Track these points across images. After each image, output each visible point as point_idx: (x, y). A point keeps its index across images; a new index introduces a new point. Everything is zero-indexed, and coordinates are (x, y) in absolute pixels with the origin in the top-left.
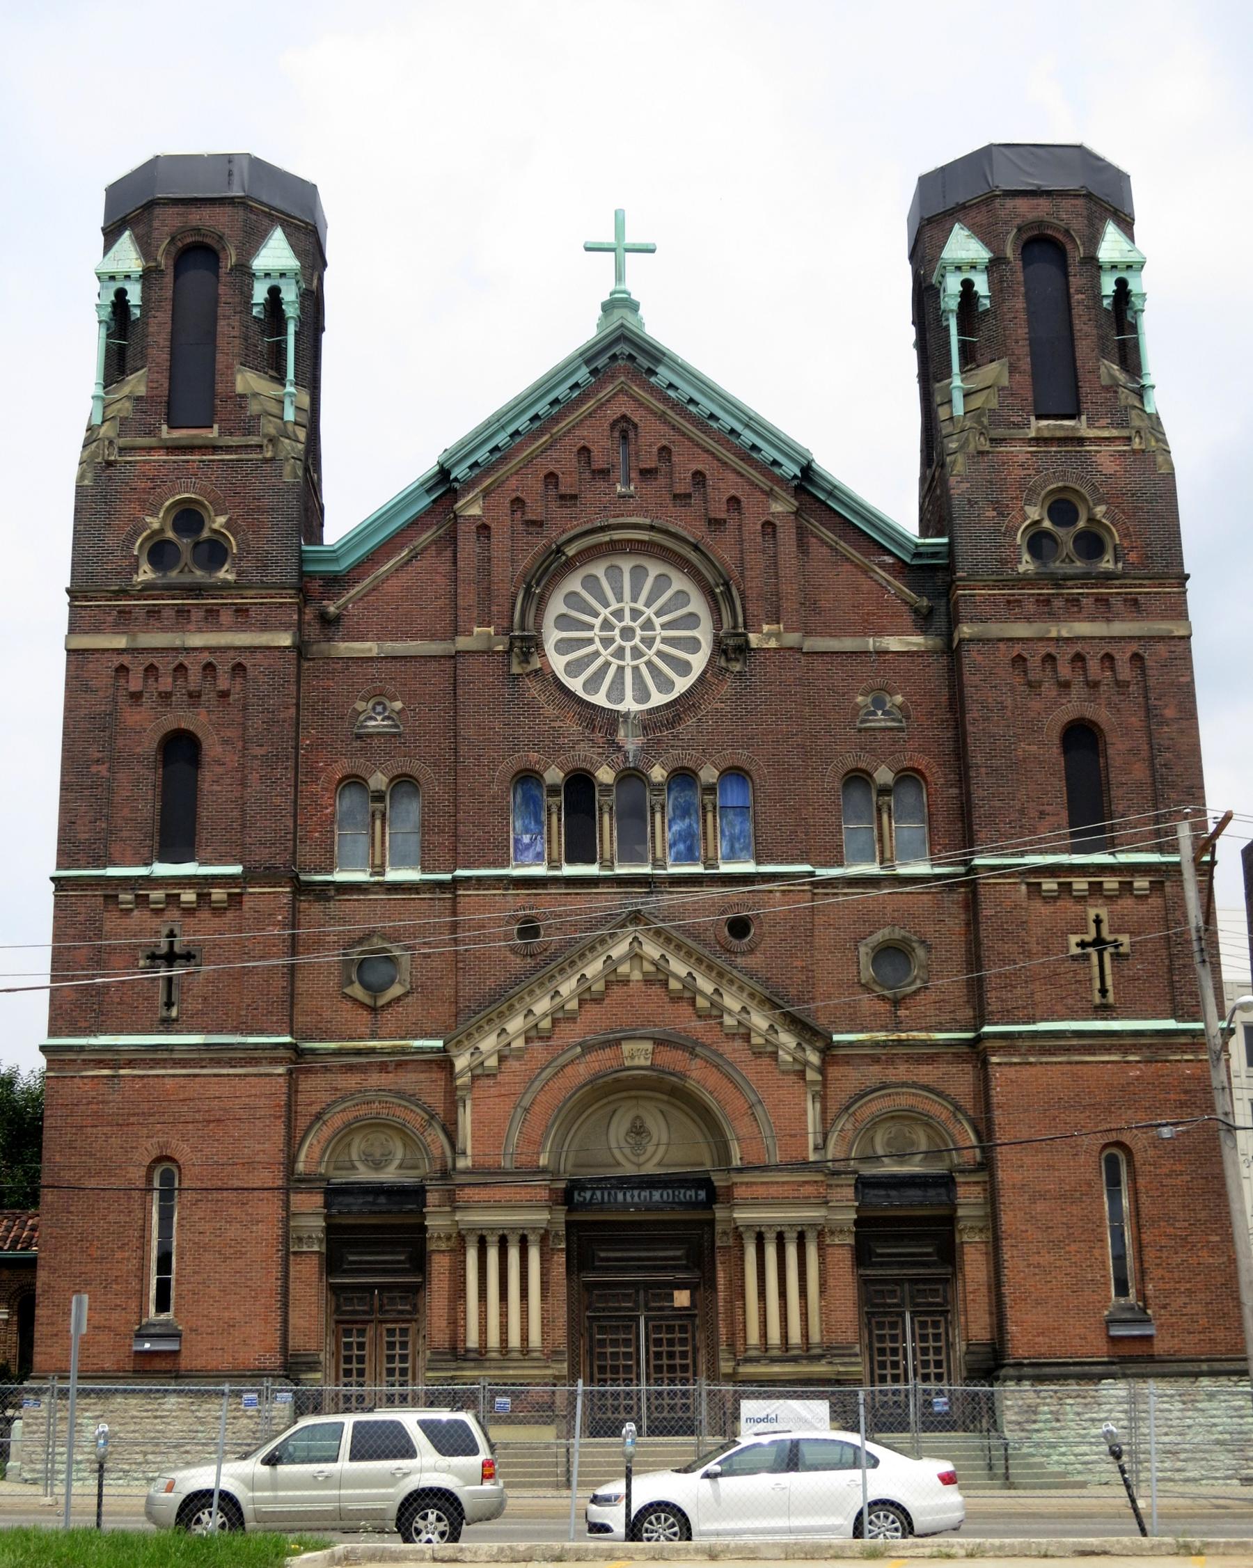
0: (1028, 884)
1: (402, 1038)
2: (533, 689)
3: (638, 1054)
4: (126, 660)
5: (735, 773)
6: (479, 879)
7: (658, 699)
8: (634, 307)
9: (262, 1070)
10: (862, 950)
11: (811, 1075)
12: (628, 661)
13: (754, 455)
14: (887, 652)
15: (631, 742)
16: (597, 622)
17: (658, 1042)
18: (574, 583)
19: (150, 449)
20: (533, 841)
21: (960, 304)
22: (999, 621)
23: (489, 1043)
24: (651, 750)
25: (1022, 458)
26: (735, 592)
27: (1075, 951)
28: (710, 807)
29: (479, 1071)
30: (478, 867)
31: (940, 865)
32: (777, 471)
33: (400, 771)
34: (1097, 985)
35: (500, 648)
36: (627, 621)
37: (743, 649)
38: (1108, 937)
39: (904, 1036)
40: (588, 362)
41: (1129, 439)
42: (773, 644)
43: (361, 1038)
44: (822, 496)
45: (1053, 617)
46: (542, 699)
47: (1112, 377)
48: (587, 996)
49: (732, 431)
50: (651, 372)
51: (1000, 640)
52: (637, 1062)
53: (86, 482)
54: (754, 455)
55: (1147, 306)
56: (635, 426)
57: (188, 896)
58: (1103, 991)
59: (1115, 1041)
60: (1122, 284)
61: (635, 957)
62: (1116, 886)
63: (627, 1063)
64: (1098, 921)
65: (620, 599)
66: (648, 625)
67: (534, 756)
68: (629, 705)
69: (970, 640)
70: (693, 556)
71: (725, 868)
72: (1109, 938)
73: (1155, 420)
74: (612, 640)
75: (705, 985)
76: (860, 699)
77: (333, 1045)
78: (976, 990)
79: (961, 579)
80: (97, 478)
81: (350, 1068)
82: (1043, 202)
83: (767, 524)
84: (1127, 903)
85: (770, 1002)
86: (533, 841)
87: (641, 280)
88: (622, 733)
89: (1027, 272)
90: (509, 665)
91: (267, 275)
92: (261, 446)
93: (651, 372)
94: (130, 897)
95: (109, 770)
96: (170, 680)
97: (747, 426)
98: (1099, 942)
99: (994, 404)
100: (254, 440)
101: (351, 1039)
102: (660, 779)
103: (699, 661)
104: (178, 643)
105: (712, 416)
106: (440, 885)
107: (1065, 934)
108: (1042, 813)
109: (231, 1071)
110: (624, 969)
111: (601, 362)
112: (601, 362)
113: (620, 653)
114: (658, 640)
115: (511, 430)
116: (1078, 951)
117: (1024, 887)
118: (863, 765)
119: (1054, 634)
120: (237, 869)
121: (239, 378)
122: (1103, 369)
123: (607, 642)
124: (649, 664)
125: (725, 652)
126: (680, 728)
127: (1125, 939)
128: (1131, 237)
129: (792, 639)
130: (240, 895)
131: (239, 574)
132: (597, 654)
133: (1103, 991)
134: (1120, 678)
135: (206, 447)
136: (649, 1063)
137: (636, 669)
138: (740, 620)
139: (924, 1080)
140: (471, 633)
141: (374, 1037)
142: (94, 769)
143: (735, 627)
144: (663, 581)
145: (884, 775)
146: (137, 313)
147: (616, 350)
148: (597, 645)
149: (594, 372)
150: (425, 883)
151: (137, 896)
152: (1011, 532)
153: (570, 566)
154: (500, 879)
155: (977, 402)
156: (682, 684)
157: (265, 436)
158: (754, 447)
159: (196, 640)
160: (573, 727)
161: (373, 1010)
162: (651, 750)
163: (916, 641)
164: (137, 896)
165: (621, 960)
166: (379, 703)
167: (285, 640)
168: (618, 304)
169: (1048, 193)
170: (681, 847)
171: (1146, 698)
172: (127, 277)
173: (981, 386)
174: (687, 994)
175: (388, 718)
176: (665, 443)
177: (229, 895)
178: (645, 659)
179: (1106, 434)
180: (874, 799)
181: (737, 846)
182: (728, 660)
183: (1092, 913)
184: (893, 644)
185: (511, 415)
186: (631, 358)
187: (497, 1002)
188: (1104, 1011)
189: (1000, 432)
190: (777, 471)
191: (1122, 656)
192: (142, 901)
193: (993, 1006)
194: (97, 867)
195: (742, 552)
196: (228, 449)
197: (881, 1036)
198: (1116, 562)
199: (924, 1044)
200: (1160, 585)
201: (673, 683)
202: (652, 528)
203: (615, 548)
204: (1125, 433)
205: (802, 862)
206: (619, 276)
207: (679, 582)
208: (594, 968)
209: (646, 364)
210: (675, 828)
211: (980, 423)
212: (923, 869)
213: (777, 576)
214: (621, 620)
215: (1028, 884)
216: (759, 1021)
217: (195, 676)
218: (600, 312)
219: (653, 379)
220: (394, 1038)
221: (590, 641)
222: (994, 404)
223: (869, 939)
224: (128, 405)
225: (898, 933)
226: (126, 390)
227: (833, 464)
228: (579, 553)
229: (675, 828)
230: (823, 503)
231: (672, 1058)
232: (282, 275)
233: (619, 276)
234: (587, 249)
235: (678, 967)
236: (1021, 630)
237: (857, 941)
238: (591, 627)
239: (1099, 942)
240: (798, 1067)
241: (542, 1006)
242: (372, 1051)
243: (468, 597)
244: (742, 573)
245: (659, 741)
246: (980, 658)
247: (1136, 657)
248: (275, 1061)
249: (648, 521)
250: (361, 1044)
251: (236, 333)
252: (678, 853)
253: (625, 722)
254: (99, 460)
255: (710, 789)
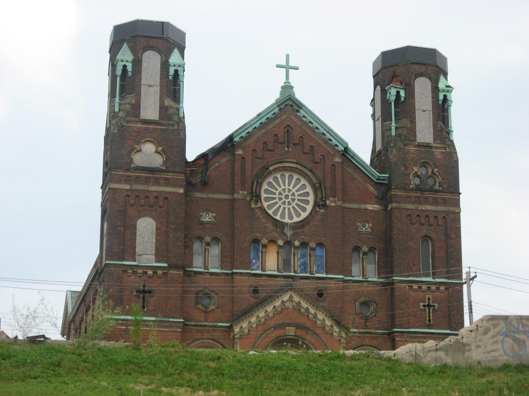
0: (409, 286)
1: (215, 322)
2: (258, 213)
3: (291, 331)
4: (129, 193)
5: (320, 245)
6: (241, 273)
7: (296, 219)
8: (292, 88)
9: (174, 329)
10: (357, 303)
11: (343, 341)
12: (286, 206)
13: (329, 142)
14: (367, 210)
15: (289, 233)
16: (277, 192)
17: (297, 328)
18: (270, 179)
19: (136, 122)
20: (256, 262)
21: (395, 99)
22: (404, 203)
23: (245, 325)
24: (295, 236)
25: (413, 151)
26: (322, 187)
27: (422, 307)
28: (312, 255)
29: (242, 334)
30: (240, 269)
31: (381, 278)
32: (336, 148)
33: (214, 236)
34: (428, 319)
35: (248, 199)
36: (287, 193)
37: (325, 206)
38: (431, 304)
39: (368, 330)
40: (278, 106)
41: (446, 148)
42: (333, 204)
43: (202, 322)
44: (349, 157)
45: (420, 203)
46: (261, 216)
47: (441, 127)
48: (275, 312)
49: (323, 133)
50: (298, 111)
51: (404, 209)
52: (291, 334)
53: (115, 132)
54: (329, 142)
55: (452, 104)
56: (292, 128)
57: (150, 272)
58: (429, 320)
59: (432, 336)
60: (445, 96)
61: (291, 299)
62: (435, 288)
63: (287, 334)
64: (429, 299)
65: (293, 188)
66: (293, 194)
67: (258, 235)
68: (287, 220)
69: (395, 208)
70: (310, 174)
71: (317, 275)
72: (432, 304)
73: (452, 141)
74: (285, 202)
75: (312, 310)
76: (358, 224)
77: (193, 323)
78: (393, 317)
79: (393, 189)
80: (118, 130)
81: (198, 331)
82: (423, 67)
83: (333, 165)
84: (438, 293)
85: (332, 317)
86: (256, 262)
87: (295, 79)
88: (286, 229)
89: (408, 76)
90: (251, 205)
91: (174, 65)
92: (173, 125)
93: (298, 111)
94: (131, 271)
95: (124, 229)
96: (144, 201)
97: (328, 132)
98: (429, 306)
99: (405, 133)
100: (172, 122)
101: (198, 321)
102: (297, 245)
103: (309, 208)
104: (146, 189)
105: (317, 128)
106: (227, 274)
107: (419, 302)
108: (414, 264)
109: (164, 329)
110: (287, 304)
111: (282, 107)
112: (282, 107)
113: (284, 203)
114: (296, 200)
115: (253, 127)
116: (423, 308)
117: (408, 287)
118: (358, 245)
119: (420, 208)
120: (165, 265)
121: (166, 100)
122: (439, 125)
123: (280, 199)
124: (293, 207)
125: (319, 206)
126: (304, 229)
127: (436, 305)
128: (447, 80)
129: (340, 203)
130: (167, 273)
131: (166, 167)
132: (277, 203)
133: (429, 320)
134: (439, 224)
135: (149, 123)
136: (293, 334)
137: (280, 206)
138: (324, 196)
139: (373, 344)
140: (239, 193)
141: (206, 321)
142: (119, 228)
143: (322, 198)
144: (298, 180)
145: (365, 249)
146: (130, 74)
147: (287, 103)
148: (277, 200)
149: (280, 110)
150: (223, 273)
151: (133, 271)
152: (409, 175)
153: (270, 173)
154: (247, 273)
155: (400, 131)
156: (304, 215)
157: (175, 121)
158: (330, 140)
159: (152, 188)
160: (270, 226)
161: (206, 312)
162: (295, 236)
163: (376, 207)
164: (133, 271)
165: (286, 301)
166: (207, 213)
167: (181, 191)
168: (287, 88)
169: (425, 64)
170: (302, 267)
171: (447, 231)
172: (127, 61)
173: (401, 126)
174: (306, 314)
175: (210, 218)
176: (301, 135)
177: (163, 273)
178: (292, 206)
179: (439, 146)
180: (260, 248)
181: (320, 268)
182: (319, 208)
183: (427, 296)
184: (370, 207)
185: (254, 122)
186: (292, 106)
187: (247, 312)
188: (429, 326)
189: (407, 142)
190: (336, 148)
191: (440, 217)
192: (135, 273)
193: (397, 322)
194: (120, 261)
195: (324, 173)
196: (163, 125)
197: (362, 330)
198: (439, 187)
199: (375, 333)
200: (453, 196)
201: (301, 214)
202: (297, 163)
203: (285, 169)
204: (445, 146)
205: (340, 274)
206: (287, 77)
207: (303, 182)
208: (278, 303)
209: (296, 108)
210: (301, 261)
211: (401, 139)
212: (375, 279)
213: (335, 182)
214: (285, 192)
215: (409, 286)
216: (328, 323)
217: (152, 200)
218: (280, 89)
219: (298, 114)
220: (212, 322)
221: (275, 198)
222: (405, 133)
223: (359, 300)
224: (128, 106)
225: (368, 299)
226: (127, 101)
227: (353, 147)
228: (273, 170)
229: (301, 261)
230: (350, 160)
231: (300, 332)
232: (179, 66)
233: (287, 77)
234: (277, 67)
235: (304, 305)
236: (410, 206)
237: (355, 301)
238: (275, 194)
239: (429, 306)
240: (339, 338)
241: (262, 314)
242: (206, 326)
243: (238, 181)
244: (324, 181)
245: (297, 233)
246: (397, 214)
247: (444, 217)
248: (178, 327)
249: (296, 161)
250: (202, 323)
251: (165, 85)
252: (301, 269)
253: (287, 226)
254: (119, 124)
255: (313, 249)
